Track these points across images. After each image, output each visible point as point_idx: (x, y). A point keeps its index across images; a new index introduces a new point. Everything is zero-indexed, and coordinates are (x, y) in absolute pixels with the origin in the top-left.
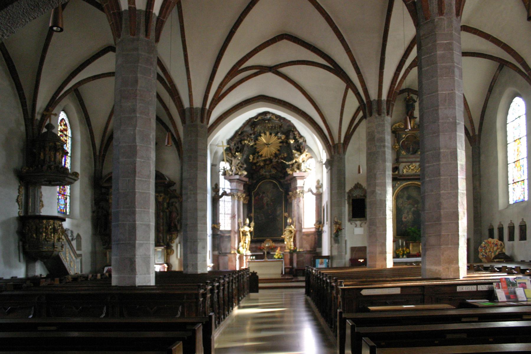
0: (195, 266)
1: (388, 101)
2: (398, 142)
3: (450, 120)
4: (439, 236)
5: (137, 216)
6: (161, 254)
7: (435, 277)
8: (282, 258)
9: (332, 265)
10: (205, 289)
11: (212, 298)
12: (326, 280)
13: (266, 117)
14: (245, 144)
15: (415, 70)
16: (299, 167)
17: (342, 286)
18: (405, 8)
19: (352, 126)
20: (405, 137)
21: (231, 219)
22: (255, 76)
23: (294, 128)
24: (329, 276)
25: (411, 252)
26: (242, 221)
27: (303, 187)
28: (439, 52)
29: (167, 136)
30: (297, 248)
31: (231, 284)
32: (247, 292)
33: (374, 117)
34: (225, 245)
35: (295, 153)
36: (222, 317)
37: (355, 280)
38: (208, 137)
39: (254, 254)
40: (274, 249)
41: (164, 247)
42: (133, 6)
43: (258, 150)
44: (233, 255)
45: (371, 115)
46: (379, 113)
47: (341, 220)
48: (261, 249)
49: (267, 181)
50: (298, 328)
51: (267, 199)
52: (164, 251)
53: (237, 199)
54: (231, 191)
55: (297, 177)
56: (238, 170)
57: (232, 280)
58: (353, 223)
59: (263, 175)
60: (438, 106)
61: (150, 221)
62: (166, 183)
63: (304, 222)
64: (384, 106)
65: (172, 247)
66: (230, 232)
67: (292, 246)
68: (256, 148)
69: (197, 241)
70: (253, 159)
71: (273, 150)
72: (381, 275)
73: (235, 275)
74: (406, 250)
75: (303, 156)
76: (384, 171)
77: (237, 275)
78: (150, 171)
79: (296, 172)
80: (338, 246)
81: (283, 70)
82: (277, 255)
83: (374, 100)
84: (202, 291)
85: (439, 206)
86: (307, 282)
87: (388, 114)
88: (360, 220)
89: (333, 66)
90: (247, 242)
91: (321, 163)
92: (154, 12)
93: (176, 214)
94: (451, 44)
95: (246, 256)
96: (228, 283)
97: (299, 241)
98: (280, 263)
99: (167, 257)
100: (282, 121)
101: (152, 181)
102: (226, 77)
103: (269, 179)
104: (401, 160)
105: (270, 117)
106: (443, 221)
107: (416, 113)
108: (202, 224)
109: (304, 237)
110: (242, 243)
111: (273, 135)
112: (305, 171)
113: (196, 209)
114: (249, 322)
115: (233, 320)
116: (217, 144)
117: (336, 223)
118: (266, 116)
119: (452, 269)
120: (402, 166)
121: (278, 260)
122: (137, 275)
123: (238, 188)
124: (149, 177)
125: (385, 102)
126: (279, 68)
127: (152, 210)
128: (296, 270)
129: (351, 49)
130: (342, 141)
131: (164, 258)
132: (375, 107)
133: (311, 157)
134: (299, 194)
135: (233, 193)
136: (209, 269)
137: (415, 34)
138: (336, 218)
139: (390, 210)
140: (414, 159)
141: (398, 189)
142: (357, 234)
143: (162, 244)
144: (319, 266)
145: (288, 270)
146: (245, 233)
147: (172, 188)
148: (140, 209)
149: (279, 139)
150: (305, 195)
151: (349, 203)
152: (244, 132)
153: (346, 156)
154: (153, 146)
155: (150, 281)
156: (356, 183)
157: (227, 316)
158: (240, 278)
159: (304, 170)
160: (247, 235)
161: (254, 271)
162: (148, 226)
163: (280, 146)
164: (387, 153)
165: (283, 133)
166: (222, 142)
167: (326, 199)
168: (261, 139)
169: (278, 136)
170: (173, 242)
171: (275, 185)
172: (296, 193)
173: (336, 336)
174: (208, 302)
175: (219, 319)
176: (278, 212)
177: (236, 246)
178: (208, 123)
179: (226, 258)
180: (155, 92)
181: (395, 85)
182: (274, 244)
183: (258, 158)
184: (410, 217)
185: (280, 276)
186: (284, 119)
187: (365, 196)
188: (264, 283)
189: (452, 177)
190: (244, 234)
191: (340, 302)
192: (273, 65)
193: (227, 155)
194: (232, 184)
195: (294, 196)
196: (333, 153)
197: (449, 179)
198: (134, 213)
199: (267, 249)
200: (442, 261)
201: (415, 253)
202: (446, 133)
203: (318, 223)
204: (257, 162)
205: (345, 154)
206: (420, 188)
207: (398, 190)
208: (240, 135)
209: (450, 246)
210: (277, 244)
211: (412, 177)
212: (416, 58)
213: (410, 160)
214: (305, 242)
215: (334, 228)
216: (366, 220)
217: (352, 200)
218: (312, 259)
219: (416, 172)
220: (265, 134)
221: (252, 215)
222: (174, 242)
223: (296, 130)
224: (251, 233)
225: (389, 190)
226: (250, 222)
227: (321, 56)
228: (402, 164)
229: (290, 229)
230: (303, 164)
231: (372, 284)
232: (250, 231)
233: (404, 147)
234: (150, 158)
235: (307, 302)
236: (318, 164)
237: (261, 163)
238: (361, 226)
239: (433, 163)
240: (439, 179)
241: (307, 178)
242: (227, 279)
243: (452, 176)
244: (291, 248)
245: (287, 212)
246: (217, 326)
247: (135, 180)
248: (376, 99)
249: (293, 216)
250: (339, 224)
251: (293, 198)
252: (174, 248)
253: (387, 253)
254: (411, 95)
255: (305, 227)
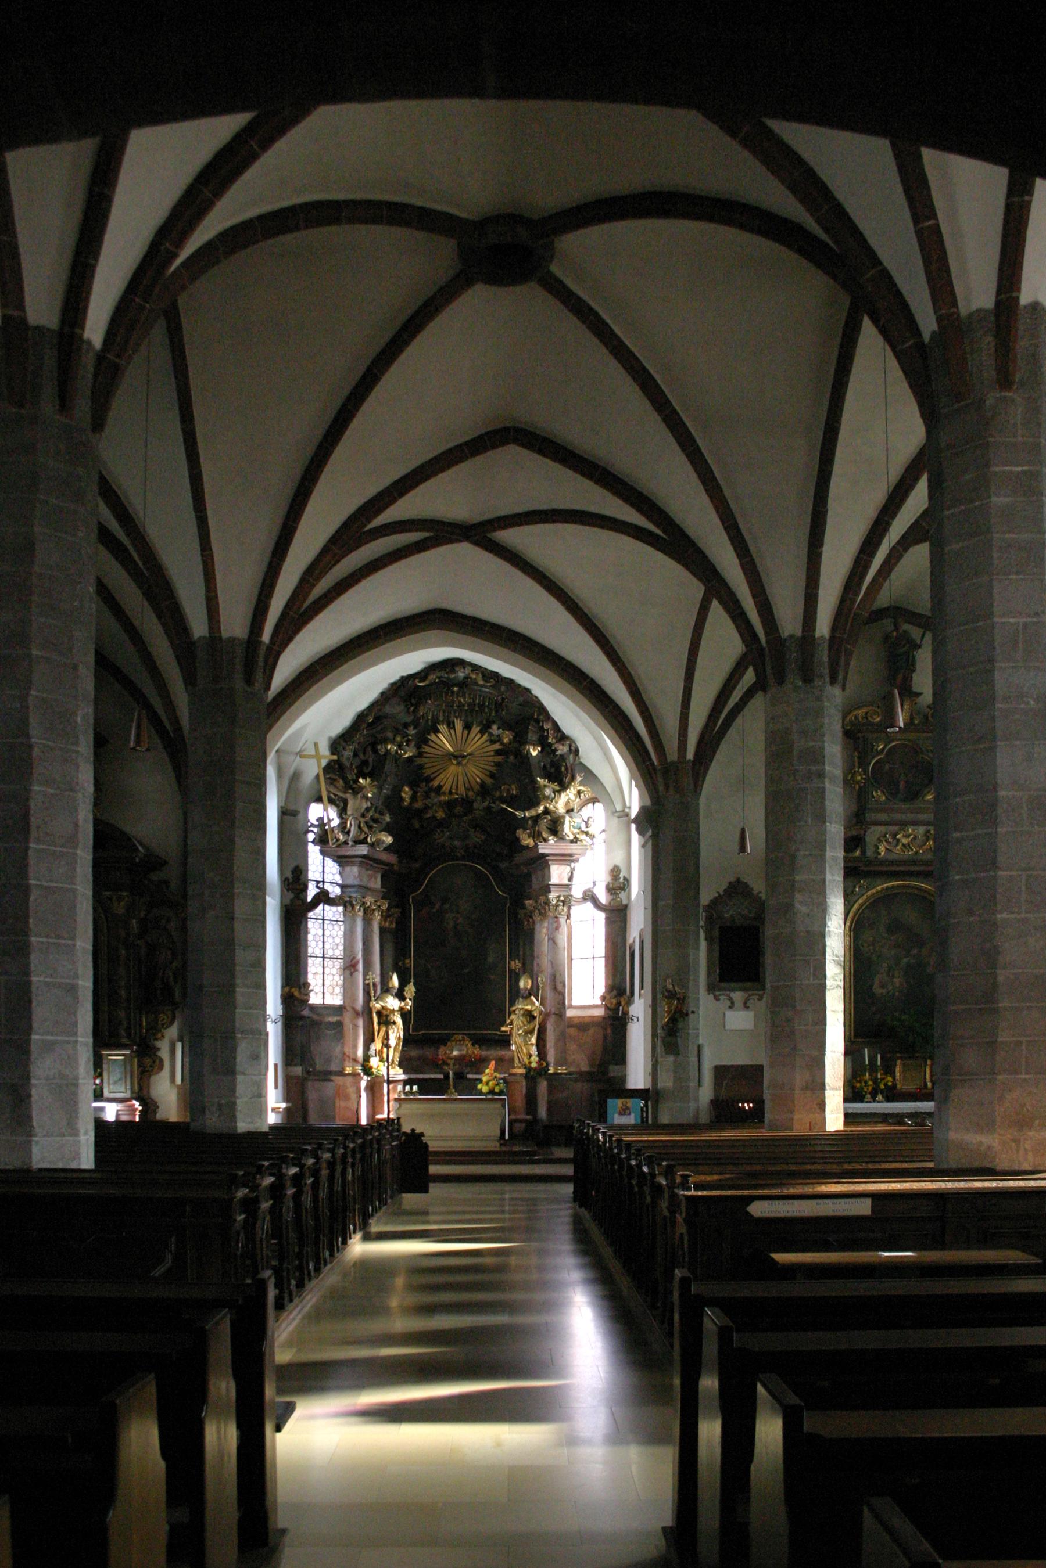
0: (229, 1110)
1: (835, 641)
2: (863, 763)
3: (1028, 703)
4: (992, 1045)
5: (35, 959)
6: (123, 1069)
7: (977, 1164)
8: (501, 1093)
9: (655, 1117)
10: (255, 1188)
11: (275, 1212)
12: (639, 1166)
13: (452, 676)
14: (388, 752)
15: (920, 554)
16: (555, 827)
17: (689, 1189)
18: (893, 363)
19: (721, 712)
20: (883, 749)
21: (344, 974)
22: (419, 551)
23: (542, 710)
24: (648, 1156)
25: (899, 1086)
26: (378, 980)
27: (568, 887)
28: (999, 500)
29: (134, 725)
30: (548, 1065)
31: (339, 1168)
32: (392, 1191)
33: (790, 686)
34: (324, 1049)
35: (545, 786)
36: (311, 1266)
37: (730, 1168)
38: (270, 727)
39: (413, 1076)
40: (478, 1065)
41: (132, 1051)
42: (16, 313)
43: (427, 772)
44: (349, 1079)
45: (781, 681)
46: (807, 676)
47: (685, 986)
48: (436, 1064)
49: (446, 867)
50: (555, 1306)
51: (458, 918)
52: (131, 1060)
53: (361, 913)
54: (342, 891)
55: (548, 855)
56: (366, 829)
57: (344, 1155)
58: (722, 998)
59: (443, 846)
60: (991, 661)
61: (76, 976)
62: (137, 860)
63: (570, 989)
64: (823, 655)
65: (159, 1049)
66: (339, 1010)
67: (535, 1059)
68: (421, 767)
69: (234, 1038)
70: (414, 798)
71: (476, 773)
72: (812, 1155)
73: (354, 1142)
74: (882, 1079)
75: (570, 794)
76: (821, 846)
77: (360, 1141)
78: (76, 825)
79: (545, 840)
80: (675, 1062)
81: (510, 537)
82: (487, 1084)
83: (791, 637)
84: (241, 1193)
85: (991, 957)
86: (580, 1162)
87: (833, 680)
88: (744, 990)
89: (664, 531)
90: (393, 1042)
91: (625, 818)
92: (87, 335)
93: (169, 953)
94: (1034, 476)
95: (389, 1082)
96: (331, 1165)
97: (556, 1044)
98: (498, 1105)
99: (140, 1079)
100: (503, 688)
101: (85, 856)
102: (325, 551)
103: (463, 858)
104: (870, 816)
105: (466, 678)
106: (1004, 1004)
107: (923, 681)
108: (248, 987)
109: (572, 1031)
110: (377, 1045)
111: (475, 729)
112: (575, 841)
113: (230, 944)
114: (400, 1281)
115: (345, 1275)
116: (298, 750)
117: (671, 995)
118: (453, 671)
119: (1029, 1142)
120: (873, 834)
121: (489, 1097)
122: (36, 1136)
123: (365, 882)
124: (72, 840)
125: (826, 645)
126: (495, 530)
127: (84, 943)
128: (545, 1127)
129: (722, 483)
130: (690, 755)
131: (132, 1083)
132: (793, 655)
133: (594, 800)
134: (557, 906)
135: (350, 897)
136: (272, 1119)
137: (924, 442)
138: (669, 981)
139: (838, 963)
140: (909, 816)
141: (860, 901)
142: (733, 1028)
143: (125, 1041)
144: (618, 1120)
145: (520, 1127)
146: (387, 1016)
147: (155, 877)
148: (44, 940)
149: (493, 742)
150: (575, 910)
151: (709, 939)
152: (386, 717)
153: (702, 800)
154: (85, 747)
155: (77, 1156)
156: (733, 879)
157: (326, 1264)
158: (368, 1151)
159: (572, 837)
160: (394, 1023)
161: (413, 1130)
162: (72, 989)
163: (498, 765)
164: (828, 795)
165: (505, 725)
166: (316, 744)
167: (638, 923)
168: (438, 741)
169: (491, 734)
170: (159, 1035)
171: (479, 874)
172: (547, 902)
173: (671, 1334)
174: (264, 1225)
175: (302, 1274)
176: (490, 959)
177: (360, 1053)
178: (268, 687)
179: (329, 1088)
180: (92, 579)
181: (857, 594)
182: (477, 1051)
183: (427, 795)
184: (897, 985)
185: (498, 1144)
186: (510, 682)
187: (760, 918)
188: (448, 1163)
189: (1034, 873)
190: (385, 1020)
191: (682, 1234)
192: (476, 518)
193: (331, 784)
194: (348, 869)
195: (540, 914)
196: (661, 788)
197: (1024, 878)
198: (23, 950)
199: (454, 1065)
200: (998, 1119)
201: (911, 1087)
202: (1018, 742)
203: (615, 992)
204: (427, 808)
205: (700, 794)
206: (932, 903)
207: (861, 906)
208: (369, 725)
209: (1023, 1076)
210: (487, 1050)
211: (902, 868)
212: (925, 513)
213: (898, 817)
214: (572, 1047)
215: (664, 1007)
216: (763, 988)
217: (722, 930)
218: (597, 1099)
219: (916, 853)
220: (451, 726)
221: (410, 962)
222: (163, 1036)
223: (548, 717)
224: (404, 1015)
225: (836, 906)
226: (403, 984)
227: (626, 500)
228: (873, 828)
229: (529, 1007)
230: (567, 818)
231: (781, 1185)
232: (401, 1009)
233: (880, 778)
234: (77, 783)
235: (577, 1224)
236: (615, 820)
237: (436, 812)
238: (746, 1007)
239: (973, 829)
240: (995, 878)
241: (581, 859)
242: (327, 1156)
243: (1029, 869)
244: (530, 1063)
245: (518, 957)
246: (294, 1293)
247: (27, 848)
248: (799, 633)
249: (535, 968)
250: (678, 999)
251: (537, 918)
252: (164, 1054)
253: (827, 1087)
254: (906, 627)
255: (574, 1003)
